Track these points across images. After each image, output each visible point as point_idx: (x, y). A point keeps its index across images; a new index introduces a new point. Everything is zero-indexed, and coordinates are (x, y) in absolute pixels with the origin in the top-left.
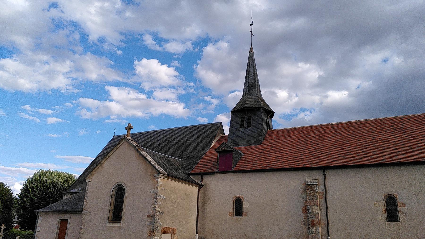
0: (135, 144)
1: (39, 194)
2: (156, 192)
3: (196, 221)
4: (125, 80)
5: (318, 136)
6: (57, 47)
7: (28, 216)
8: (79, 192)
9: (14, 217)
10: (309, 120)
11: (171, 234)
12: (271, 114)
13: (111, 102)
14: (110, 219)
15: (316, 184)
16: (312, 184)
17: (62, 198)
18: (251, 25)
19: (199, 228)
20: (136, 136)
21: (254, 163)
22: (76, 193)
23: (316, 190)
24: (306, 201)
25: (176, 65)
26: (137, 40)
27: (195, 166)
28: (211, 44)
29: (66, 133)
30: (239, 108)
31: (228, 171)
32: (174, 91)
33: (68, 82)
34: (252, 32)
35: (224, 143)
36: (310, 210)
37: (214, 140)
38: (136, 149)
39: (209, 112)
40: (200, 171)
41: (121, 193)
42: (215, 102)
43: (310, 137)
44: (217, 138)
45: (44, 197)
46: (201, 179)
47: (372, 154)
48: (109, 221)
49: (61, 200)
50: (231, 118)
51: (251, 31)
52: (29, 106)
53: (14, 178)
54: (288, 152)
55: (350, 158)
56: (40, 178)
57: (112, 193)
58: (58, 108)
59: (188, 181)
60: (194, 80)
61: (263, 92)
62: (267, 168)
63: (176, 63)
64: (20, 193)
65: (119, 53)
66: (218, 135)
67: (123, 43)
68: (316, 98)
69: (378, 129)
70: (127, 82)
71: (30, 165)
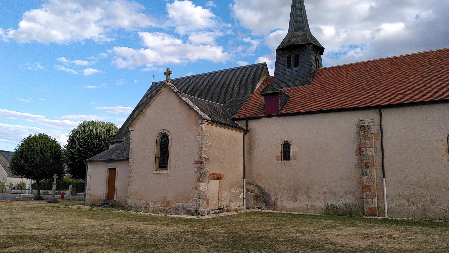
0: (176, 90)
1: (85, 144)
2: (201, 138)
3: (243, 166)
4: (158, 26)
5: (373, 72)
7: (78, 166)
8: (123, 141)
9: (64, 167)
10: (359, 58)
11: (219, 180)
12: (321, 50)
13: (147, 50)
14: (157, 167)
15: (370, 124)
16: (366, 124)
17: (108, 148)
20: (176, 82)
21: (302, 105)
22: (120, 142)
23: (371, 130)
24: (360, 143)
25: (211, 5)
29: (104, 84)
30: (285, 46)
33: (101, 30)
36: (364, 152)
37: (258, 83)
38: (177, 94)
40: (244, 116)
41: (165, 141)
42: (255, 43)
43: (365, 74)
45: (90, 147)
46: (246, 124)
47: (437, 89)
48: (156, 168)
49: (107, 150)
50: (276, 58)
52: (65, 57)
53: (59, 131)
54: (339, 91)
55: (409, 95)
56: (84, 129)
58: (94, 58)
59: (233, 127)
64: (67, 144)
66: (262, 77)
68: (367, 33)
69: (445, 61)
70: (161, 27)
71: (73, 117)
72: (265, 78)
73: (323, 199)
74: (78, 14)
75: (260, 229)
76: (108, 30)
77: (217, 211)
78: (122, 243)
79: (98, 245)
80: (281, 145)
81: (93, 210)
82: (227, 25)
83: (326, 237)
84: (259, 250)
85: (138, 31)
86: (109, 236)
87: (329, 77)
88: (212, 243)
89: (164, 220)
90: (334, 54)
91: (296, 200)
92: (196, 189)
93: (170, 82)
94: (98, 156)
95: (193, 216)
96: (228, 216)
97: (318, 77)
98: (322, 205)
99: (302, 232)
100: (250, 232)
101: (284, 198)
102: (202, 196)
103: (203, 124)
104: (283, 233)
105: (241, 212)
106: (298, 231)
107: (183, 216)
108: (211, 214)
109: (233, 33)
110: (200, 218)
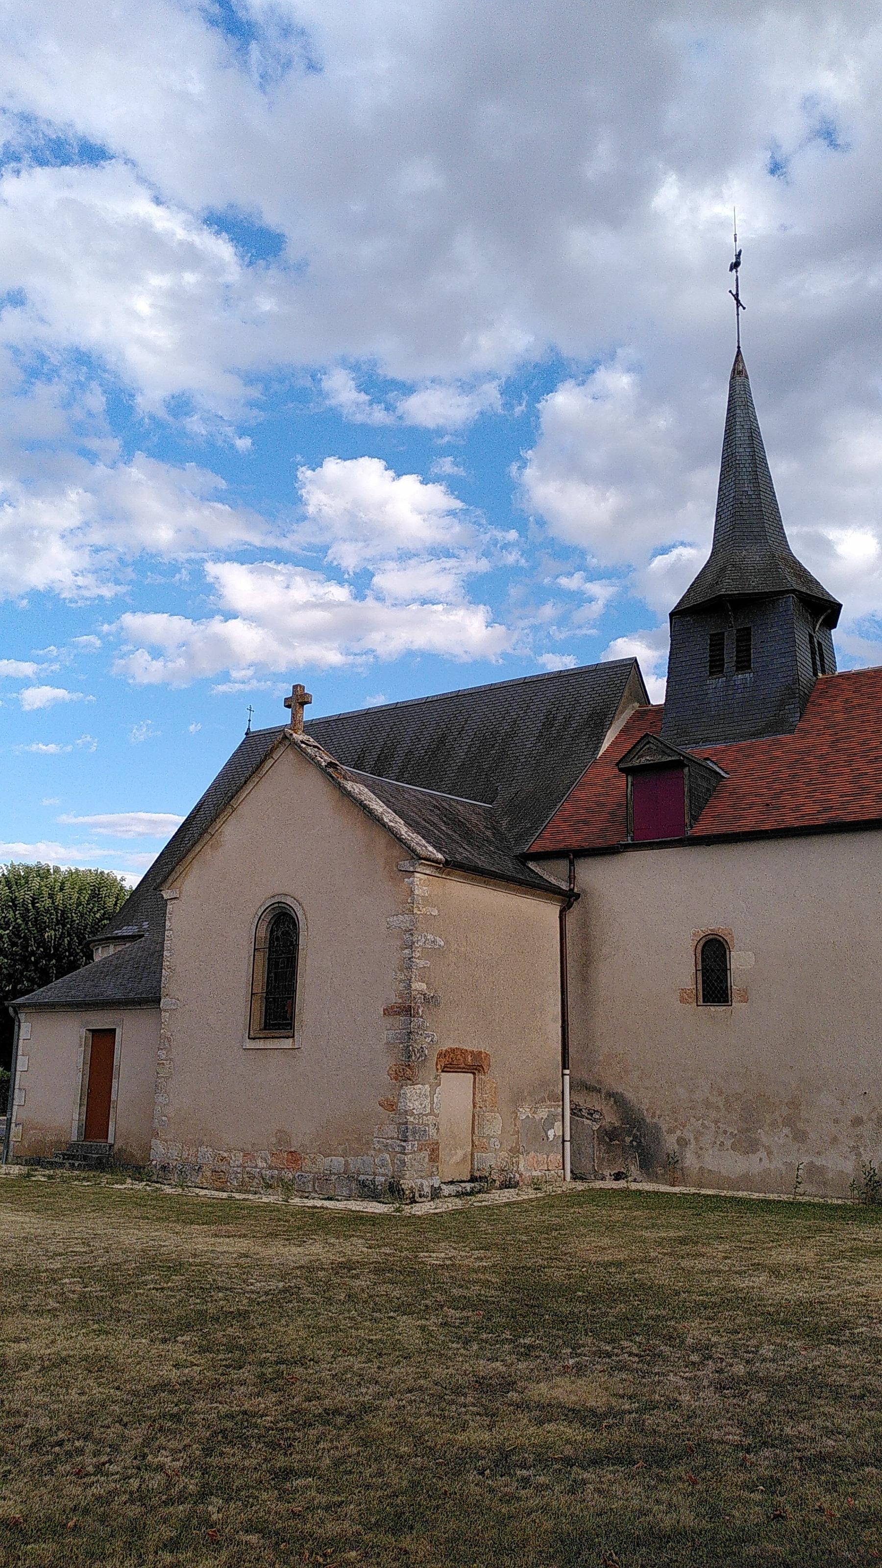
0: (324, 758)
1: (13, 944)
4: (271, 542)
6: (33, 445)
8: (143, 936)
11: (474, 1073)
12: (829, 611)
13: (232, 623)
14: (255, 1026)
17: (90, 957)
18: (735, 266)
19: (572, 1050)
21: (768, 805)
22: (133, 938)
26: (301, 396)
27: (544, 825)
28: (570, 384)
29: (88, 739)
30: (700, 600)
31: (669, 839)
32: (450, 563)
33: (83, 560)
34: (737, 294)
35: (647, 735)
37: (609, 728)
38: (329, 773)
39: (577, 632)
40: (562, 845)
42: (601, 591)
44: (621, 719)
48: (251, 1032)
49: (86, 964)
50: (672, 640)
51: (734, 293)
57: (254, 934)
58: (55, 653)
60: (520, 523)
61: (790, 530)
62: (817, 823)
63: (447, 466)
65: (243, 444)
66: (625, 708)
67: (255, 412)
72: (633, 712)
73: (852, 1144)
74: (9, 510)
75: (621, 1257)
76: (106, 557)
77: (468, 1186)
78: (124, 1307)
79: (39, 1312)
80: (693, 949)
81: (34, 1179)
82: (503, 533)
83: (863, 1289)
84: (613, 1341)
85: (204, 561)
86: (80, 1278)
87: (859, 705)
88: (445, 1308)
89: (279, 1220)
90: (877, 622)
91: (752, 1147)
92: (391, 1106)
93: (306, 731)
94: (55, 988)
95: (379, 1202)
96: (507, 1204)
97: (821, 704)
98: (849, 1166)
99: (774, 1271)
100: (583, 1267)
101: (708, 1139)
102: (414, 1133)
103: (415, 874)
104: (703, 1272)
105: (555, 1189)
106: (758, 1267)
107: (345, 1202)
108: (445, 1197)
109: (523, 561)
110: (407, 1210)
